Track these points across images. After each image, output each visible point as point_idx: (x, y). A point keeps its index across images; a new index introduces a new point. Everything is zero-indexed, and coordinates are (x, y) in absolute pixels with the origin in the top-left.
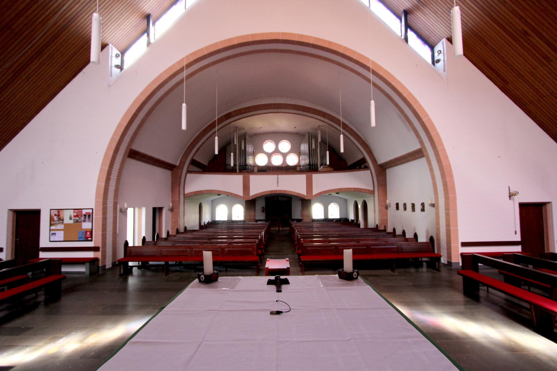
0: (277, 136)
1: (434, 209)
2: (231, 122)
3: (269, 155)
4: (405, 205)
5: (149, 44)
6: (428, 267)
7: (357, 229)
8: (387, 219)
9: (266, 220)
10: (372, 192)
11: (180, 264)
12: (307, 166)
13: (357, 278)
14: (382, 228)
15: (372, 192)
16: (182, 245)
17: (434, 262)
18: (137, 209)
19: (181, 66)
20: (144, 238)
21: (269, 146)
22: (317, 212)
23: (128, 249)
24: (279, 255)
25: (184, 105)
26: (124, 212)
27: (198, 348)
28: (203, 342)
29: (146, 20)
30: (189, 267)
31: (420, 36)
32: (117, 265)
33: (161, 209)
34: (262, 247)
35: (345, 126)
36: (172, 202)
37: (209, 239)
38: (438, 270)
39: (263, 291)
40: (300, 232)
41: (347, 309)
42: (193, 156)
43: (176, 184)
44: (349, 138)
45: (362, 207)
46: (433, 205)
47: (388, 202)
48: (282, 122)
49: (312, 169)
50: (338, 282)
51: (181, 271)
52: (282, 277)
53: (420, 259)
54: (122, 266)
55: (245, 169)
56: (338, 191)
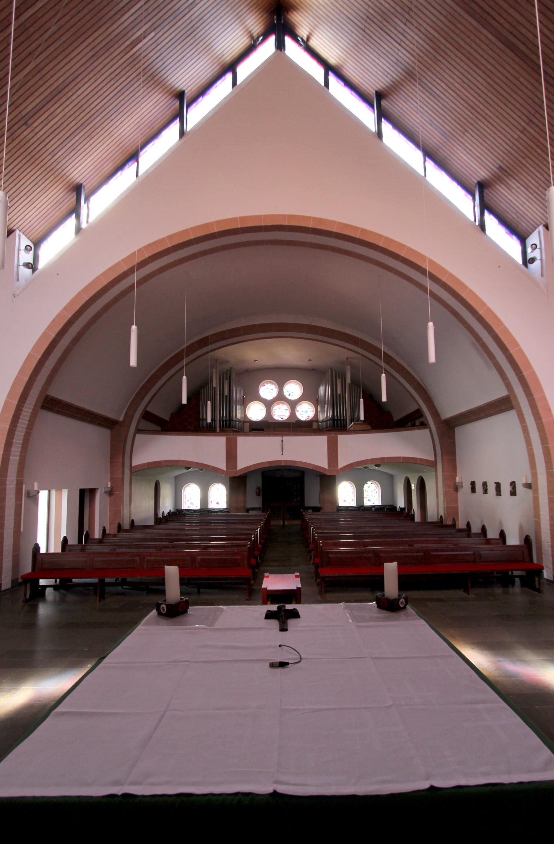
0: (280, 374)
1: (530, 492)
2: (207, 353)
3: (269, 404)
4: (485, 484)
5: (78, 230)
6: (522, 585)
7: (409, 523)
8: (458, 507)
10: (433, 464)
11: (123, 583)
12: (329, 422)
13: (405, 608)
14: (449, 523)
15: (433, 464)
16: (127, 550)
17: (532, 577)
18: (53, 492)
19: (131, 265)
20: (65, 540)
21: (268, 390)
22: (345, 495)
23: (39, 558)
24: (283, 569)
25: (134, 327)
26: (33, 498)
27: (160, 721)
28: (167, 712)
29: (75, 193)
30: (137, 587)
31: (503, 221)
32: (20, 584)
33: (92, 491)
34: (257, 553)
35: (389, 360)
36: (112, 480)
37: (171, 541)
38: (539, 591)
39: (260, 629)
40: (317, 528)
41: (389, 658)
42: (147, 406)
43: (119, 451)
44: (396, 378)
45: (417, 487)
46: (528, 486)
47: (458, 480)
48: (289, 351)
49: (335, 426)
50: (375, 615)
51: (123, 594)
52: (289, 607)
53: (510, 573)
54: (29, 585)
55: (231, 427)
56: (379, 462)
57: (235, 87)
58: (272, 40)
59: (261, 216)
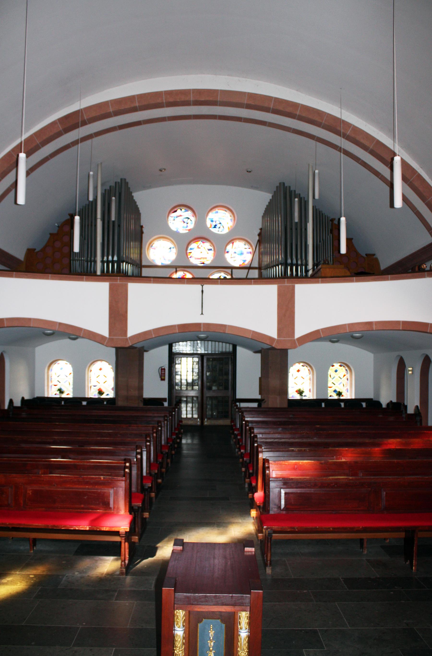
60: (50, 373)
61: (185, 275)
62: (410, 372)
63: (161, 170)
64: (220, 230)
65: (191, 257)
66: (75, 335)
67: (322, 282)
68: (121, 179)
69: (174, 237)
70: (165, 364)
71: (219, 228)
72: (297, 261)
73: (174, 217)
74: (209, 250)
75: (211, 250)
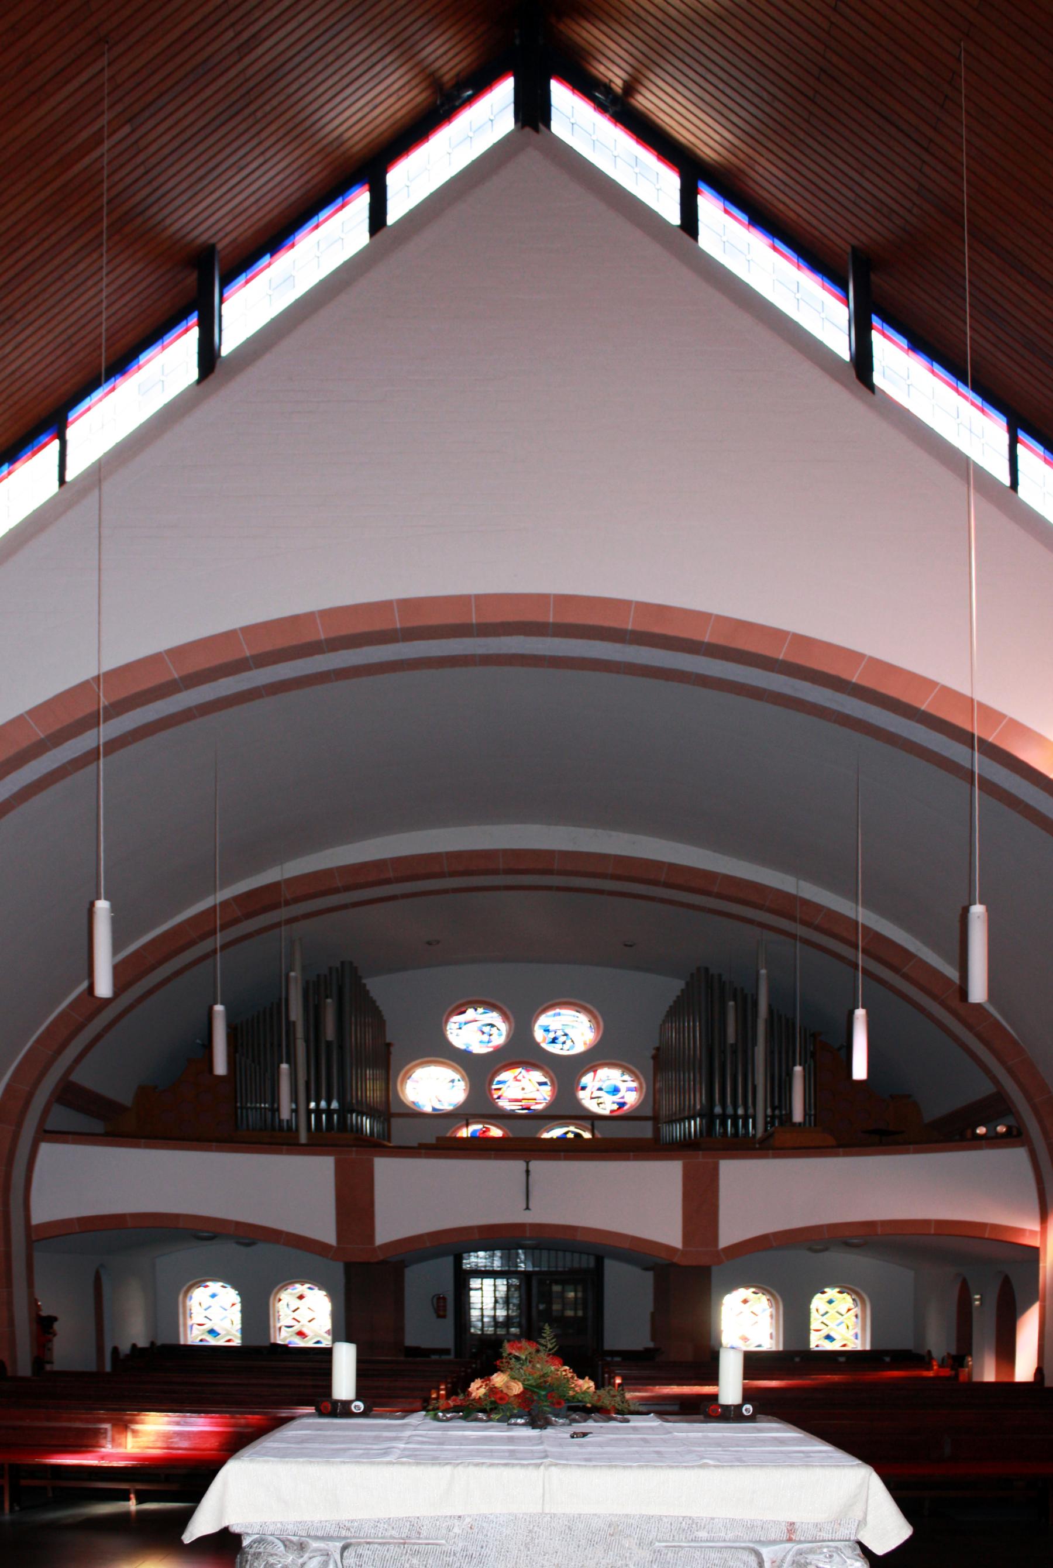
9: (471, 1289)
42: (70, 1070)
57: (380, 235)
58: (505, 90)
59: (468, 597)
60: (188, 1303)
61: (488, 1130)
62: (977, 1303)
63: (429, 943)
64: (566, 1047)
65: (499, 1098)
66: (207, 1232)
67: (775, 1156)
68: (343, 963)
69: (462, 1059)
70: (448, 1288)
71: (564, 1043)
72: (735, 1108)
73: (460, 1024)
74: (541, 1084)
75: (545, 1084)
